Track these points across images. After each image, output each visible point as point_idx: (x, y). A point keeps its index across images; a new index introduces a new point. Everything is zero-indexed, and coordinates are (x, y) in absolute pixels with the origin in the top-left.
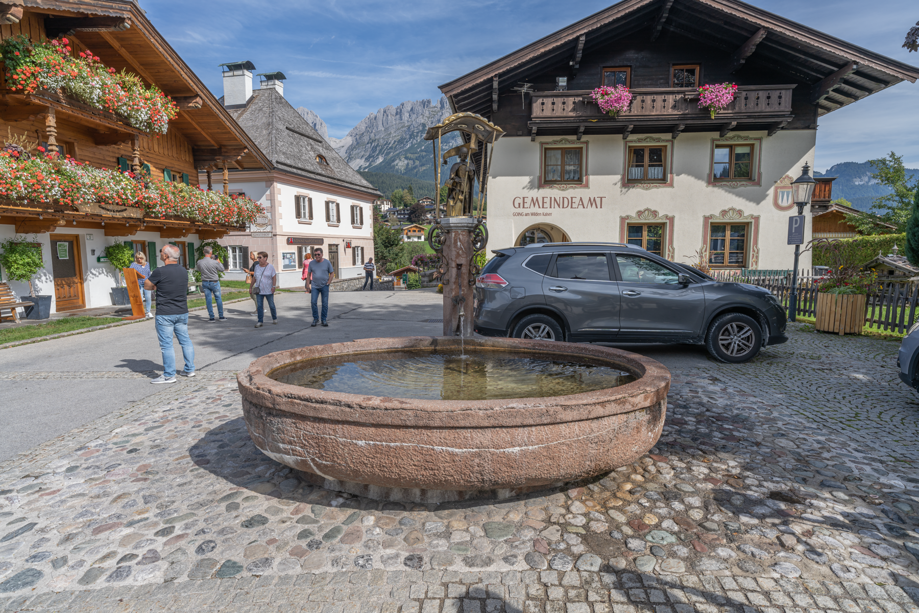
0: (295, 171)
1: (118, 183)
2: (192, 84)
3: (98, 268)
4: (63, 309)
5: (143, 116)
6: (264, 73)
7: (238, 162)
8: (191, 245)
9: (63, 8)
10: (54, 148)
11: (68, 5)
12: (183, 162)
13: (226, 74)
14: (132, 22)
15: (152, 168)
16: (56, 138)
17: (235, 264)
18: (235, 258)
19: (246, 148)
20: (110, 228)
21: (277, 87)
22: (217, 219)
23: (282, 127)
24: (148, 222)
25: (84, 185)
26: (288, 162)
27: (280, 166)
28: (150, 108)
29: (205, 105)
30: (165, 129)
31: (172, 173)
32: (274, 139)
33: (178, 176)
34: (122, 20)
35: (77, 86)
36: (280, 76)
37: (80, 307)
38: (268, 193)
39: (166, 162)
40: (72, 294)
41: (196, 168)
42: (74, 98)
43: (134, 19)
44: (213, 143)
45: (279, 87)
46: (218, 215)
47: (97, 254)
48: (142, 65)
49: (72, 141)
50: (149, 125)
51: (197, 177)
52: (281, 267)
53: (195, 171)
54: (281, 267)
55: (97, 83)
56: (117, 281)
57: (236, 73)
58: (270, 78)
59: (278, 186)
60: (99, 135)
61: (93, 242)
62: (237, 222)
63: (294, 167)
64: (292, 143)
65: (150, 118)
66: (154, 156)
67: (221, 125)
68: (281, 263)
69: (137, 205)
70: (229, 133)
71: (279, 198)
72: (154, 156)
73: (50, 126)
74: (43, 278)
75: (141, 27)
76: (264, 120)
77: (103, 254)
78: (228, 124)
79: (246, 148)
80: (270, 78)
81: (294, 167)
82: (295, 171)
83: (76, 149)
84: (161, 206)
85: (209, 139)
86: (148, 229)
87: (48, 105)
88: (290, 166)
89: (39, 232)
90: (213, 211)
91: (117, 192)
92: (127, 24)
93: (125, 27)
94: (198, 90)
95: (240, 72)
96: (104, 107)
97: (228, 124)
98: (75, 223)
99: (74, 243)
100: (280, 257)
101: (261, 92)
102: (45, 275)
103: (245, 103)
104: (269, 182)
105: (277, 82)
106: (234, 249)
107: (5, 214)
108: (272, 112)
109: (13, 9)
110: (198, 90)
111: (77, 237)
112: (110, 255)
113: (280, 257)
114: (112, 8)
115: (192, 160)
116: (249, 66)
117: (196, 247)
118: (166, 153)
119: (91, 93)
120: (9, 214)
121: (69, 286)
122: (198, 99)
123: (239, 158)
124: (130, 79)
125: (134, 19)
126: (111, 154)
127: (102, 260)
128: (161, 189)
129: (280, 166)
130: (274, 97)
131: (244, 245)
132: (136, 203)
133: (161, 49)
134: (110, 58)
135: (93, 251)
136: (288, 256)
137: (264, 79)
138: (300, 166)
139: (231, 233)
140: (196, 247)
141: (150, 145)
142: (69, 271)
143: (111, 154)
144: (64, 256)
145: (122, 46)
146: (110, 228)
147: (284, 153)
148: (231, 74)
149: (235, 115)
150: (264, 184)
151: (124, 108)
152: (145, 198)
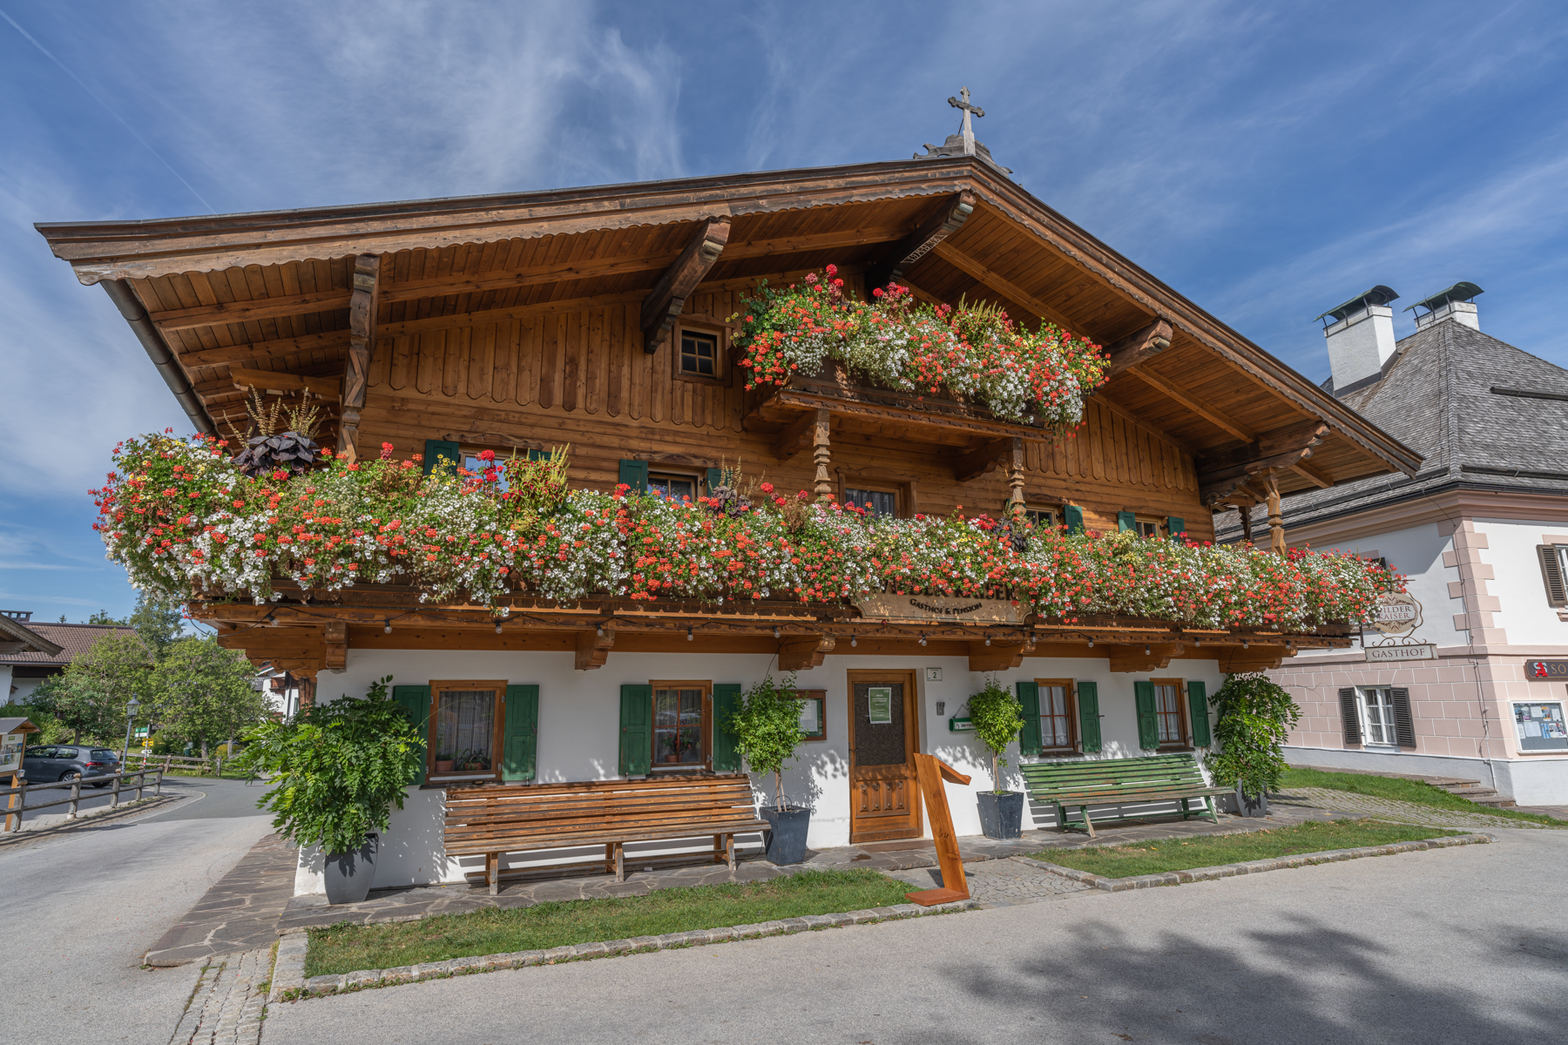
0: (1527, 481)
1: (943, 542)
2: (1138, 294)
3: (954, 746)
4: (863, 838)
5: (1013, 386)
6: (1423, 300)
7: (1302, 464)
8: (1197, 687)
9: (814, 203)
10: (825, 488)
11: (824, 196)
12: (1171, 490)
13: (1331, 331)
14: (975, 195)
15: (1086, 514)
16: (828, 466)
17: (1377, 731)
18: (1375, 716)
19: (1320, 422)
20: (982, 651)
21: (1458, 317)
22: (1236, 614)
23: (1476, 390)
24: (1045, 633)
25: (852, 553)
26: (1502, 464)
27: (1474, 478)
28: (1050, 368)
29: (1180, 339)
30: (1076, 411)
31: (1143, 521)
32: (1454, 421)
33: (1158, 524)
34: (955, 198)
35: (860, 351)
36: (1465, 292)
37: (910, 834)
38: (1449, 548)
39: (1125, 498)
40: (895, 805)
41: (1204, 503)
42: (868, 383)
43: (979, 189)
44: (1243, 437)
45: (1466, 315)
46: (1241, 604)
47: (950, 711)
48: (1035, 295)
49: (906, 479)
50: (1032, 407)
51: (1211, 523)
52: (1513, 745)
53: (1202, 510)
54: (1513, 745)
55: (898, 336)
56: (1000, 779)
57: (1351, 320)
58: (1435, 304)
59: (1475, 528)
60: (947, 452)
61: (943, 686)
62: (1310, 620)
63: (1523, 474)
64: (1512, 422)
65: (1035, 386)
66: (1095, 488)
67: (1239, 380)
68: (1513, 734)
69: (1001, 591)
70: (1267, 395)
71: (1482, 558)
72: (1095, 488)
73: (818, 446)
74: (829, 768)
75: (998, 201)
76: (1428, 389)
77: (964, 713)
78: (1255, 369)
79: (1320, 422)
80: (1435, 304)
81: (1523, 474)
82: (1527, 481)
83: (914, 493)
84: (1061, 589)
85: (1222, 425)
86: (1191, 653)
87: (817, 405)
88: (1510, 473)
89: (799, 667)
90: (1218, 594)
91: (936, 565)
92: (967, 205)
93: (963, 213)
94: (1156, 305)
95: (1362, 314)
96: (917, 384)
97: (1255, 369)
98: (854, 643)
99: (905, 688)
100: (1507, 717)
101: (1417, 338)
102: (833, 761)
103: (1378, 370)
104: (1449, 521)
105: (1456, 305)
106: (1371, 696)
107: (705, 630)
108: (1446, 368)
109: (711, 227)
110: (1156, 305)
111: (912, 674)
112: (975, 716)
113: (1507, 717)
114: (925, 180)
115: (1193, 486)
116: (1382, 295)
117: (1210, 691)
118: (1181, 486)
119: (883, 359)
120: (714, 631)
121: (891, 786)
122: (1161, 327)
123: (1306, 452)
124: (974, 315)
125: (979, 189)
126: (991, 495)
127: (959, 725)
128: (1109, 552)
129: (1474, 478)
130: (1449, 335)
131: (1396, 683)
132: (987, 586)
133: (1050, 235)
134: (944, 288)
135: (941, 706)
136: (1537, 712)
137: (1422, 311)
138: (1543, 467)
139: (1302, 655)
140: (1210, 691)
141: (1084, 465)
142: (884, 753)
143: (991, 495)
144: (880, 714)
145: (990, 269)
146: (982, 651)
147: (1486, 447)
148: (1342, 325)
149: (1354, 403)
150: (1432, 530)
151: (967, 378)
152: (1014, 573)
